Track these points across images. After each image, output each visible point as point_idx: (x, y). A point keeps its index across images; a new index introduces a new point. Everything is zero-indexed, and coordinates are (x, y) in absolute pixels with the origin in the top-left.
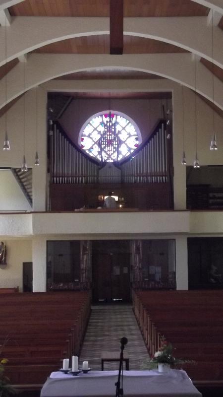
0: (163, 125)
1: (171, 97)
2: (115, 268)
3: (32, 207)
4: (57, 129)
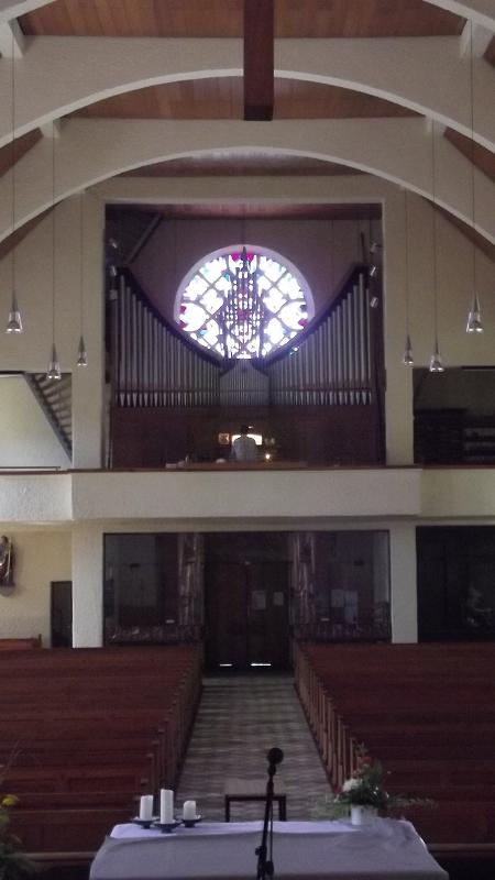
0: (361, 276)
1: (379, 216)
2: (254, 593)
3: (71, 459)
4: (126, 285)
